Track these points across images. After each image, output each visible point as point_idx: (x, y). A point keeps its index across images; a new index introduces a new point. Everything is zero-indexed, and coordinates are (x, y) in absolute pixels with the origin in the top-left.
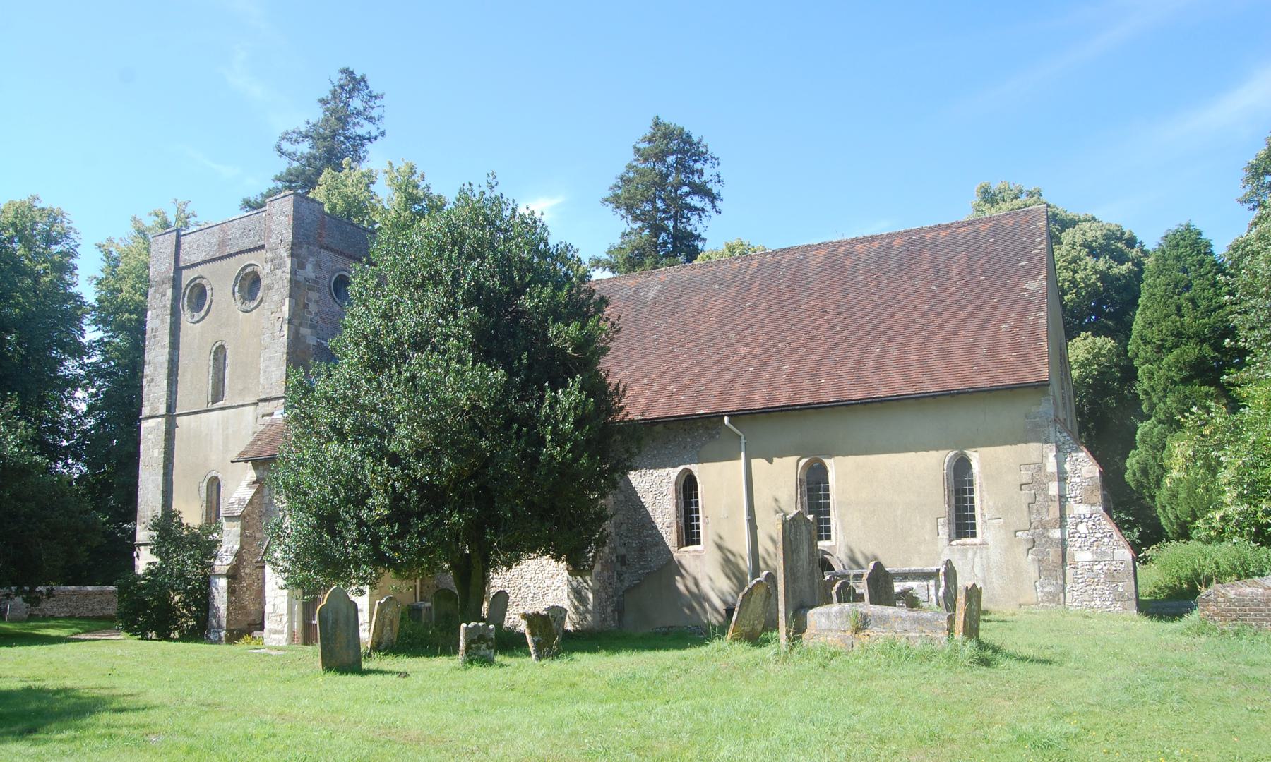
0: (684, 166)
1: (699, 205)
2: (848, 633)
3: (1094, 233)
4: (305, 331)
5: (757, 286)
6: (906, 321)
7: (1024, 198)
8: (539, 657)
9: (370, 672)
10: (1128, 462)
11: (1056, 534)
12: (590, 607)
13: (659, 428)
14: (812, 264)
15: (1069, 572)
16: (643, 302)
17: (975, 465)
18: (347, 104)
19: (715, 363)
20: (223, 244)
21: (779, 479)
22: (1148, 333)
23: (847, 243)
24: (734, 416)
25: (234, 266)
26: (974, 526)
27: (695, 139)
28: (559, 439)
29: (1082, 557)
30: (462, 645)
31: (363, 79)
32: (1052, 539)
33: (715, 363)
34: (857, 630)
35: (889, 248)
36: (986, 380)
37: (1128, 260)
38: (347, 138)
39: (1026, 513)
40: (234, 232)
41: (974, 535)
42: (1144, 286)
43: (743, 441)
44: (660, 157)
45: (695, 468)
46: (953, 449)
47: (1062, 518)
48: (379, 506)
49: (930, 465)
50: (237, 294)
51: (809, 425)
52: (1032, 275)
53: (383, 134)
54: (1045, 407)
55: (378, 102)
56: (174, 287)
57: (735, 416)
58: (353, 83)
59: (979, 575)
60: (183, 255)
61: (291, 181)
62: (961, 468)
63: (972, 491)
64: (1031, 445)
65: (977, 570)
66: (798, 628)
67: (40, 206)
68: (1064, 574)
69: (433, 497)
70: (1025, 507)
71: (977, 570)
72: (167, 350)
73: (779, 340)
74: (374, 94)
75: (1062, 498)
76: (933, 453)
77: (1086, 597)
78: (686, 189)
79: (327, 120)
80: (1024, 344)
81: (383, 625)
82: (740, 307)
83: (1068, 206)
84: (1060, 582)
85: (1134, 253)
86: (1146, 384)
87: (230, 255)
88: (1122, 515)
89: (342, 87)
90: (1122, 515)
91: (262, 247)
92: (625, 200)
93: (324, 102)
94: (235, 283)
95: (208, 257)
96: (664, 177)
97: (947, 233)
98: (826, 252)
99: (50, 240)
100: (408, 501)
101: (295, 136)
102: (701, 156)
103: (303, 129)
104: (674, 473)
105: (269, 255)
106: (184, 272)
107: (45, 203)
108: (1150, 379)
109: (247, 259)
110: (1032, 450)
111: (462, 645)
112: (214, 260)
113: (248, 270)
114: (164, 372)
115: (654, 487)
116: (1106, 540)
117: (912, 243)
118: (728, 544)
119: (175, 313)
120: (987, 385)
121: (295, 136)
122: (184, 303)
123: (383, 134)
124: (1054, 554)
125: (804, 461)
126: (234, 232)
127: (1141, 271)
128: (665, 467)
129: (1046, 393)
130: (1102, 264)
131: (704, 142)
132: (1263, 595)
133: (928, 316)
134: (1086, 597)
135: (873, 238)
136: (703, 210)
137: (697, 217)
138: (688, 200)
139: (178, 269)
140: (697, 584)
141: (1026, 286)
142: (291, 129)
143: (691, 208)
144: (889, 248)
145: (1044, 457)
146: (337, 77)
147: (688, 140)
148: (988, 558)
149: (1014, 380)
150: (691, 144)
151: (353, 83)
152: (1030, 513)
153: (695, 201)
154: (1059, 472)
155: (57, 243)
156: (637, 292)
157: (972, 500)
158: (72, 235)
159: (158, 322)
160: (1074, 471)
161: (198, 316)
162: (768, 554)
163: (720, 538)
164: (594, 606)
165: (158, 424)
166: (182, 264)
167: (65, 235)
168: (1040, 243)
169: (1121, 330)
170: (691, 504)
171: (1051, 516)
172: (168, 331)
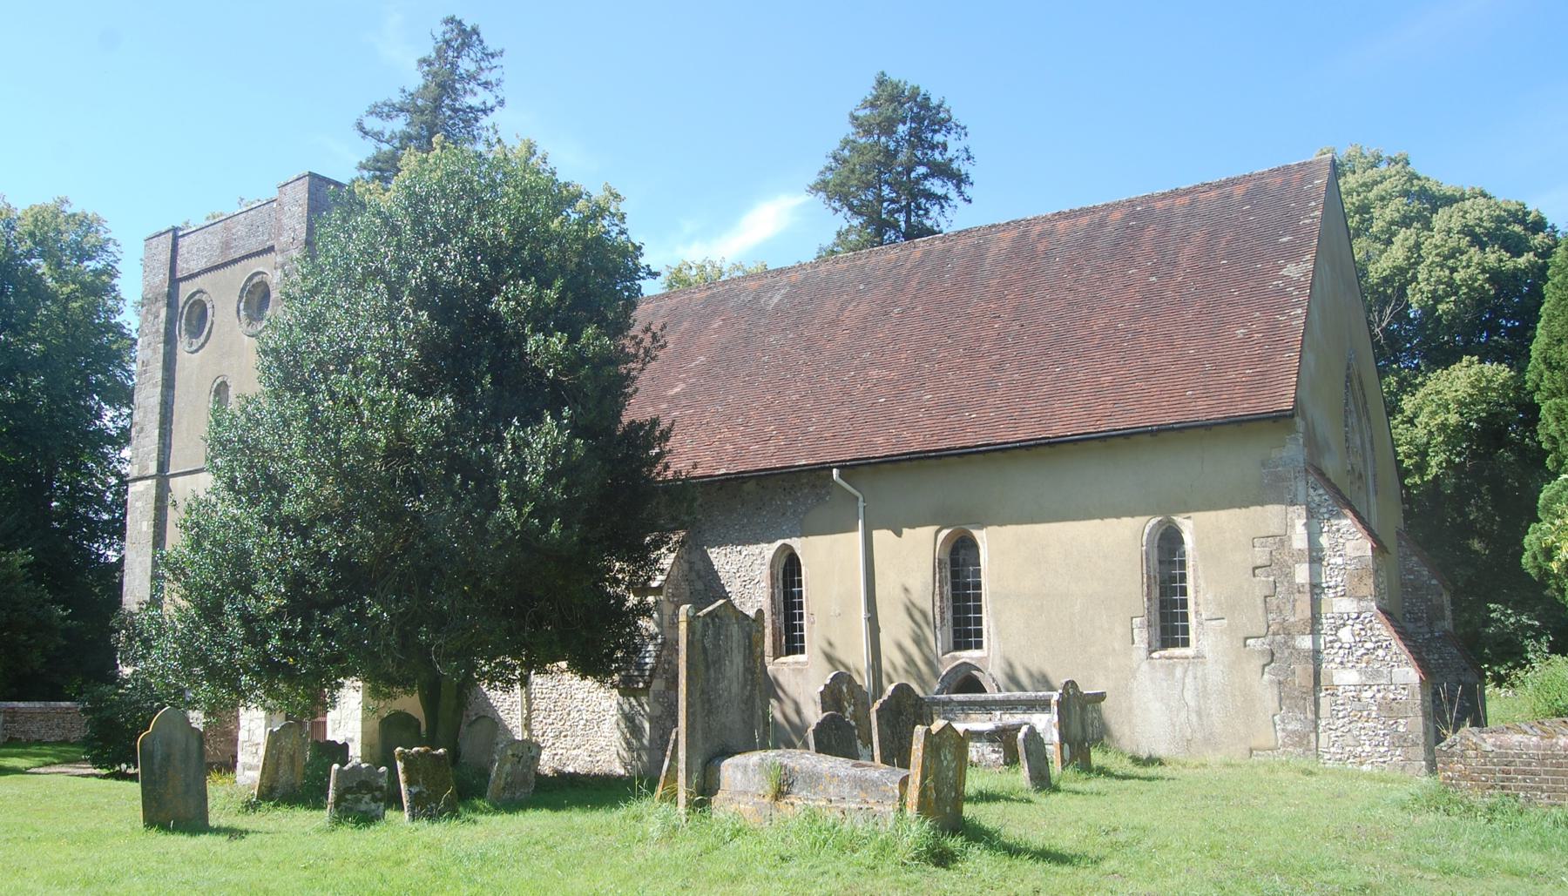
0: (920, 139)
1: (939, 191)
2: (767, 800)
3: (1476, 211)
5: (914, 284)
6: (1105, 328)
7: (1383, 167)
8: (413, 817)
9: (1103, 771)
10: (1526, 540)
11: (1305, 642)
12: (645, 742)
13: (750, 486)
14: (994, 250)
15: (1325, 702)
16: (762, 312)
17: (1187, 537)
18: (454, 66)
19: (835, 393)
20: (226, 245)
21: (909, 557)
22: (1554, 354)
23: (1047, 220)
24: (844, 467)
25: (238, 276)
26: (1186, 630)
27: (934, 102)
28: (520, 494)
29: (1345, 678)
30: (331, 794)
31: (475, 31)
32: (1299, 651)
33: (835, 393)
34: (780, 794)
35: (1102, 224)
36: (1202, 410)
37: (1529, 249)
38: (456, 111)
39: (1260, 611)
40: (240, 230)
41: (1186, 643)
42: (1548, 288)
43: (861, 504)
44: (888, 127)
45: (797, 544)
46: (1155, 514)
47: (1315, 618)
48: (270, 597)
49: (1120, 539)
50: (242, 313)
51: (952, 481)
52: (1293, 254)
53: (501, 103)
54: (1292, 450)
55: (495, 62)
56: (169, 305)
57: (849, 468)
58: (463, 37)
59: (1192, 704)
60: (180, 264)
61: (379, 169)
62: (1168, 546)
63: (1183, 577)
64: (1269, 507)
65: (1188, 695)
66: (706, 788)
67: (69, 211)
68: (1317, 703)
69: (352, 578)
70: (1260, 602)
71: (1188, 695)
72: (159, 389)
73: (927, 360)
74: (490, 50)
75: (1316, 589)
76: (1126, 520)
77: (1349, 739)
78: (922, 170)
79: (426, 87)
80: (1267, 355)
81: (278, 765)
82: (886, 313)
83: (1443, 176)
84: (1310, 716)
85: (1538, 239)
86: (1553, 428)
87: (235, 261)
88: (1524, 619)
89: (447, 42)
90: (1524, 619)
91: (271, 249)
92: (836, 190)
93: (424, 61)
94: (241, 297)
95: (209, 265)
96: (891, 155)
97: (1186, 200)
98: (1015, 233)
99: (83, 255)
100: (313, 586)
101: (386, 109)
102: (943, 124)
103: (397, 99)
104: (769, 550)
105: (279, 259)
106: (182, 285)
107: (75, 208)
108: (1557, 420)
109: (256, 265)
110: (1270, 516)
111: (331, 794)
112: (217, 267)
113: (256, 280)
114: (155, 417)
115: (744, 571)
116: (1381, 652)
117: (1134, 216)
118: (840, 654)
119: (170, 340)
120: (1202, 417)
121: (386, 109)
123: (501, 103)
124: (1301, 674)
125: (945, 532)
126: (240, 230)
127: (1546, 267)
128: (757, 542)
129: (1291, 429)
130: (1492, 257)
131: (946, 106)
132: (1538, 747)
133: (1137, 319)
134: (1349, 739)
135: (1083, 212)
136: (946, 198)
137: (937, 207)
138: (928, 184)
139: (174, 281)
140: (798, 712)
141: (1284, 272)
142: (380, 99)
143: (930, 196)
144: (1102, 224)
145: (1289, 526)
146: (440, 30)
147: (925, 104)
148: (1205, 679)
149: (1242, 409)
150: (928, 108)
151: (463, 37)
152: (1267, 611)
153: (936, 186)
154: (1311, 549)
155: (91, 258)
156: (757, 298)
157: (1184, 591)
158: (111, 248)
159: (149, 352)
160: (1333, 547)
161: (197, 343)
162: (895, 669)
163: (830, 644)
164: (651, 741)
165: (148, 488)
166: (179, 275)
167: (102, 247)
168: (1316, 208)
169: (1516, 355)
170: (792, 594)
171: (1299, 616)
172: (160, 364)
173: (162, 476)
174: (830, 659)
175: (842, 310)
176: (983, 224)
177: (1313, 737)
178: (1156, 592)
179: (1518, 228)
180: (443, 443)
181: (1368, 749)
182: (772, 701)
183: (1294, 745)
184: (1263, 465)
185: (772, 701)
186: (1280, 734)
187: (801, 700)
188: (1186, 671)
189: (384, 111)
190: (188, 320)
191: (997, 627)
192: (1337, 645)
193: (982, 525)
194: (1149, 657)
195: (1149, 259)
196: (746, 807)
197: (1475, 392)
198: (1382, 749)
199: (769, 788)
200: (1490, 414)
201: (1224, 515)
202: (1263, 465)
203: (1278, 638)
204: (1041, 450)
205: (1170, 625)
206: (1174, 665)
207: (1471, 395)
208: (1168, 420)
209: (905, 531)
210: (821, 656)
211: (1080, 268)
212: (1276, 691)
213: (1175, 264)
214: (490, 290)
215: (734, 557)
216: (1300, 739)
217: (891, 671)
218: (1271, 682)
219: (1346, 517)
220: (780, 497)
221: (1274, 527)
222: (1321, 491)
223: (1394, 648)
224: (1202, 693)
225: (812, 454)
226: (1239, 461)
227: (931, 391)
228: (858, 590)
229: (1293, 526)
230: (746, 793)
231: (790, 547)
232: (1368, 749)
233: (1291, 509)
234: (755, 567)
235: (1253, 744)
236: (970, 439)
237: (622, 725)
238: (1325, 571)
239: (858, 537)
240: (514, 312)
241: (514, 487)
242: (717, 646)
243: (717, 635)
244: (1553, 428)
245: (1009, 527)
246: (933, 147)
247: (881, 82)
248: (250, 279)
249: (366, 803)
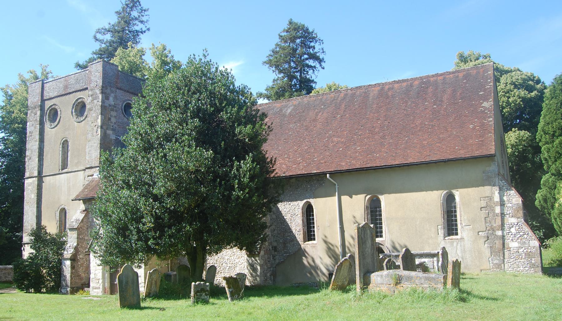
1: (313, 65)
2: (392, 285)
3: (516, 77)
4: (109, 132)
5: (343, 106)
6: (421, 124)
7: (481, 60)
8: (232, 299)
9: (145, 308)
11: (499, 233)
12: (258, 273)
13: (293, 180)
14: (372, 94)
15: (507, 253)
16: (284, 115)
18: (130, 14)
19: (322, 147)
20: (66, 87)
21: (355, 206)
26: (457, 230)
27: (311, 30)
28: (242, 187)
29: (513, 245)
30: (192, 294)
32: (497, 236)
34: (397, 284)
35: (411, 86)
36: (462, 154)
37: (535, 90)
38: (130, 32)
39: (483, 223)
40: (72, 81)
41: (457, 234)
43: (337, 187)
44: (293, 40)
45: (312, 201)
46: (445, 190)
47: (503, 225)
48: (148, 223)
49: (434, 198)
50: (74, 113)
51: (370, 178)
54: (493, 168)
56: (41, 110)
57: (332, 174)
59: (460, 255)
61: (101, 54)
62: (450, 200)
65: (459, 252)
66: (366, 283)
69: (176, 217)
70: (483, 219)
71: (459, 252)
75: (503, 215)
78: (306, 56)
79: (119, 22)
80: (482, 134)
81: (152, 284)
82: (335, 117)
84: (502, 258)
85: (538, 86)
87: (70, 93)
89: (127, 5)
91: (87, 89)
94: (73, 107)
95: (59, 94)
96: (295, 50)
97: (442, 77)
98: (379, 88)
100: (163, 220)
103: (107, 27)
104: (301, 203)
105: (90, 93)
110: (486, 190)
111: (192, 294)
113: (79, 101)
114: (36, 154)
116: (525, 236)
118: (330, 240)
119: (42, 124)
120: (463, 156)
121: (103, 30)
123: (148, 29)
124: (498, 243)
125: (369, 196)
126: (72, 81)
128: (296, 200)
130: (523, 93)
131: (315, 32)
135: (404, 81)
136: (315, 67)
137: (312, 71)
139: (43, 101)
140: (314, 261)
142: (101, 27)
144: (411, 86)
145: (493, 193)
147: (306, 31)
148: (464, 246)
149: (477, 153)
152: (486, 222)
153: (311, 62)
154: (500, 201)
156: (281, 110)
157: (456, 216)
162: (350, 245)
163: (326, 237)
164: (260, 273)
165: (33, 181)
166: (45, 98)
168: (490, 82)
171: (497, 224)
172: (38, 133)
173: (40, 177)
174: (326, 242)
175: (317, 115)
176: (366, 84)
177: (503, 265)
178: (446, 217)
179: (531, 82)
180: (211, 167)
181: (522, 269)
182: (304, 258)
183: (496, 268)
184: (484, 172)
185: (304, 258)
186: (491, 265)
187: (315, 257)
188: (458, 244)
189: (106, 31)
190: (49, 116)
191: (388, 229)
192: (510, 234)
193: (382, 194)
194: (444, 239)
195: (432, 99)
196: (384, 288)
197: (517, 141)
198: (527, 269)
199: (393, 282)
200: (523, 150)
201: (470, 190)
202: (484, 172)
203: (490, 232)
204: (405, 167)
205: (451, 228)
206: (453, 242)
207: (516, 142)
208: (451, 157)
209: (354, 196)
210: (322, 241)
211: (407, 102)
212: (489, 250)
213: (442, 101)
214: (219, 110)
215: (287, 206)
216: (498, 266)
217: (349, 246)
218: (488, 247)
219: (512, 190)
220: (309, 184)
221: (488, 194)
222: (504, 181)
223: (530, 234)
224: (464, 251)
225: (318, 169)
226: (475, 171)
227: (359, 146)
228: (335, 218)
229: (494, 194)
230: (382, 284)
231: (309, 202)
232: (522, 269)
233: (493, 187)
234: (296, 209)
235: (482, 268)
236: (378, 164)
237: (249, 268)
238: (506, 209)
239: (336, 198)
240: (229, 118)
241: (212, 181)
242: (365, 237)
243: (364, 235)
244: (546, 155)
245: (392, 194)
246: (310, 48)
247: (291, 23)
248: (77, 100)
249: (204, 296)
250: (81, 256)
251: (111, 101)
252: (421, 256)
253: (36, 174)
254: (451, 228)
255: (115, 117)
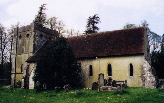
4: (36, 43)
20: (24, 30)
112: (16, 58)
122: (18, 38)
205: (131, 74)
250: (27, 78)
251: (36, 34)
252: (118, 82)
253: (15, 54)
254: (131, 74)
255: (38, 38)
